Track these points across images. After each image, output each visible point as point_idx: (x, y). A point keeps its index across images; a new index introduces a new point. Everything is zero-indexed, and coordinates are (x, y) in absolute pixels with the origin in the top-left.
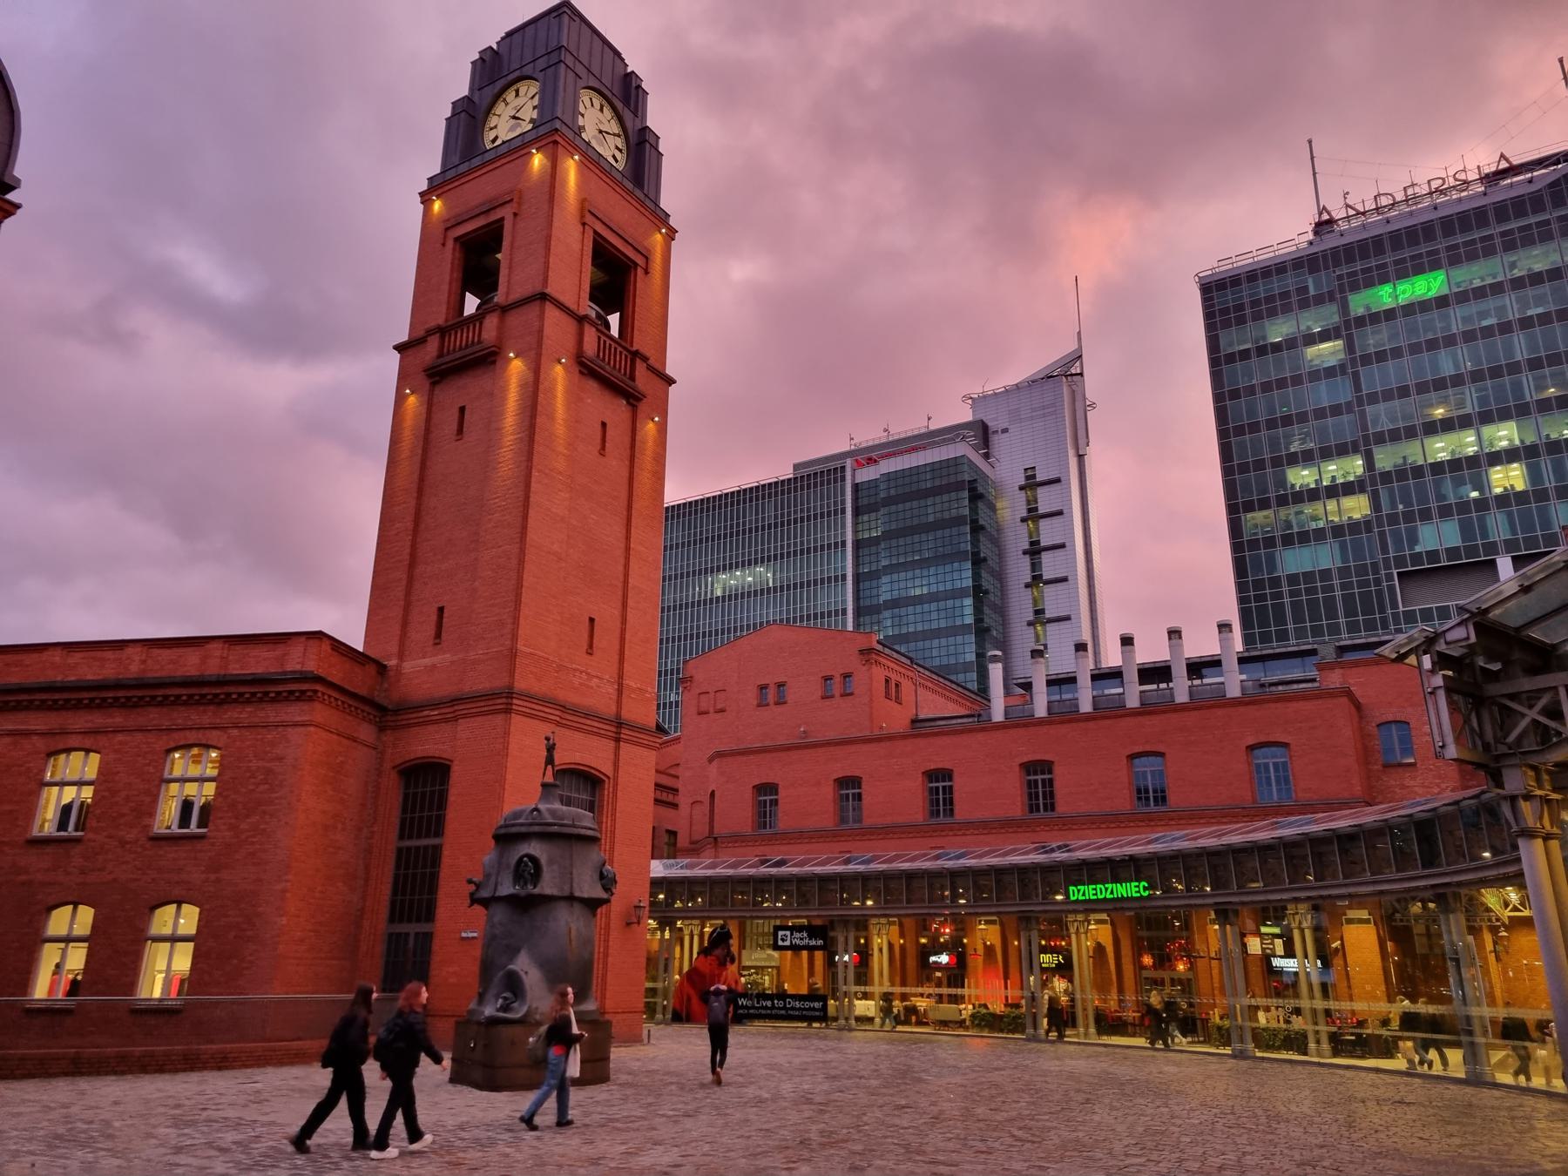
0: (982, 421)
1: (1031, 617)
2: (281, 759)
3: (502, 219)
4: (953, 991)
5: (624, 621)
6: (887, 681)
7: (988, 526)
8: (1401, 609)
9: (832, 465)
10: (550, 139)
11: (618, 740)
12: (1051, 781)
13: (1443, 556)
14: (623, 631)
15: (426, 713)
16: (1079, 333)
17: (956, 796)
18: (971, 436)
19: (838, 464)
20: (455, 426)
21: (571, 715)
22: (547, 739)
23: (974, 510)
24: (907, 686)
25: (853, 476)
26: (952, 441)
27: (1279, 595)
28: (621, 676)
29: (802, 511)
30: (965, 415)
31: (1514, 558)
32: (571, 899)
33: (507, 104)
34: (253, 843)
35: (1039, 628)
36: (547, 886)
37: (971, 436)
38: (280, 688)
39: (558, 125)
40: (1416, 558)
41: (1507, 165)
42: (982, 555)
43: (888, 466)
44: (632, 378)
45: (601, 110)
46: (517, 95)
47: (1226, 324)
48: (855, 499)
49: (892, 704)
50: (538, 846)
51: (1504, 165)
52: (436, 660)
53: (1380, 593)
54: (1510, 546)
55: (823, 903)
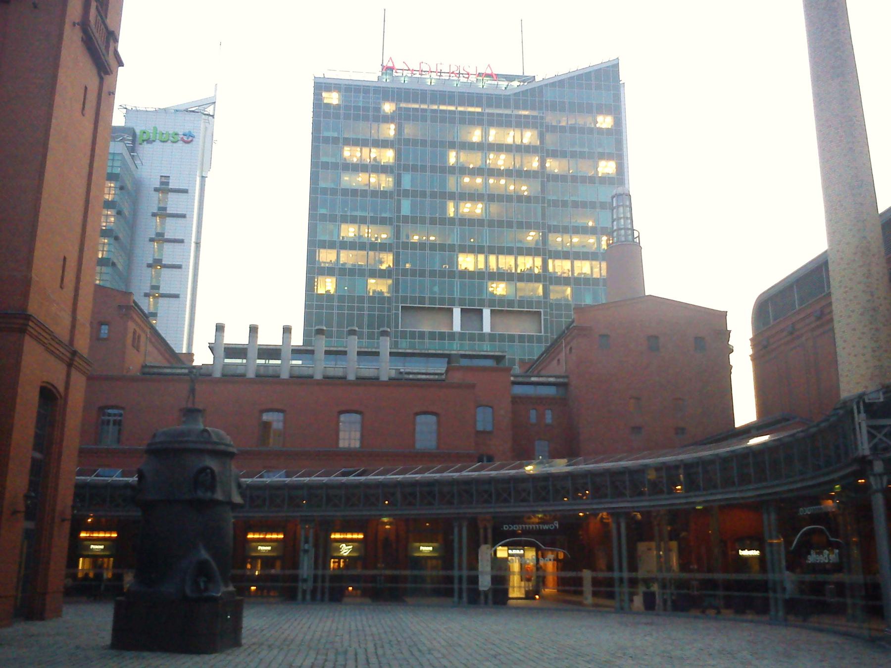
4: (456, 581)
8: (400, 329)
13: (516, 304)
18: (129, 140)
31: (491, 310)
35: (151, 300)
37: (129, 140)
54: (461, 302)
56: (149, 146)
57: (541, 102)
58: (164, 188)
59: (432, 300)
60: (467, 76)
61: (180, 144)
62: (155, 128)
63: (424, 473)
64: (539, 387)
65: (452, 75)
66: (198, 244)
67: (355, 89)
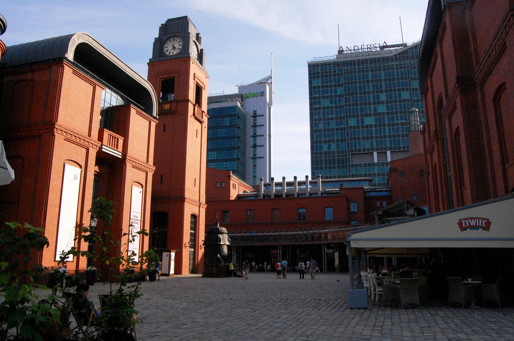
7: (241, 127)
24: (237, 185)
27: (322, 157)
30: (235, 91)
33: (171, 42)
40: (356, 150)
41: (386, 45)
44: (202, 118)
46: (174, 40)
47: (314, 77)
51: (385, 45)
53: (346, 158)
54: (377, 149)
55: (321, 234)
56: (248, 99)
57: (407, 57)
58: (255, 116)
59: (364, 150)
60: (375, 48)
61: (259, 97)
62: (250, 92)
63: (275, 233)
64: (381, 193)
65: (368, 49)
66: (270, 136)
67: (325, 64)
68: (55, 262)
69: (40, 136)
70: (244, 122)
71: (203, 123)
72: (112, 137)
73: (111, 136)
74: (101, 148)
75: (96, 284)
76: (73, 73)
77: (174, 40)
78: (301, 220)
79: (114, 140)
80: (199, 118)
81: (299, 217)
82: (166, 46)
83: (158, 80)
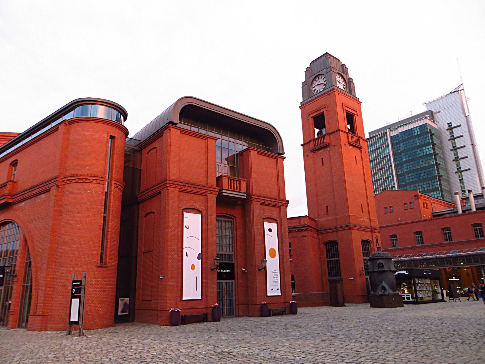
0: (431, 111)
1: (456, 170)
2: (304, 244)
3: (324, 112)
5: (368, 203)
6: (423, 203)
9: (382, 132)
10: (333, 91)
11: (372, 232)
12: (481, 229)
14: (368, 206)
15: (328, 230)
16: (461, 76)
17: (452, 234)
18: (428, 117)
19: (384, 131)
20: (321, 163)
21: (362, 228)
22: (376, 238)
23: (432, 139)
24: (429, 204)
25: (390, 134)
26: (422, 119)
28: (370, 217)
29: (374, 147)
30: (424, 109)
32: (390, 271)
33: (316, 81)
34: (302, 262)
36: (386, 269)
38: (301, 229)
39: (334, 87)
42: (436, 153)
43: (401, 130)
45: (339, 77)
46: (319, 79)
48: (391, 141)
49: (426, 209)
50: (382, 261)
52: (328, 218)
58: (451, 128)
68: (182, 302)
69: (160, 193)
70: (440, 138)
71: (361, 148)
72: (232, 181)
73: (231, 180)
74: (220, 193)
75: (222, 321)
76: (181, 133)
77: (319, 79)
78: (478, 237)
79: (235, 183)
80: (357, 145)
81: (422, 239)
82: (313, 87)
83: (310, 119)
